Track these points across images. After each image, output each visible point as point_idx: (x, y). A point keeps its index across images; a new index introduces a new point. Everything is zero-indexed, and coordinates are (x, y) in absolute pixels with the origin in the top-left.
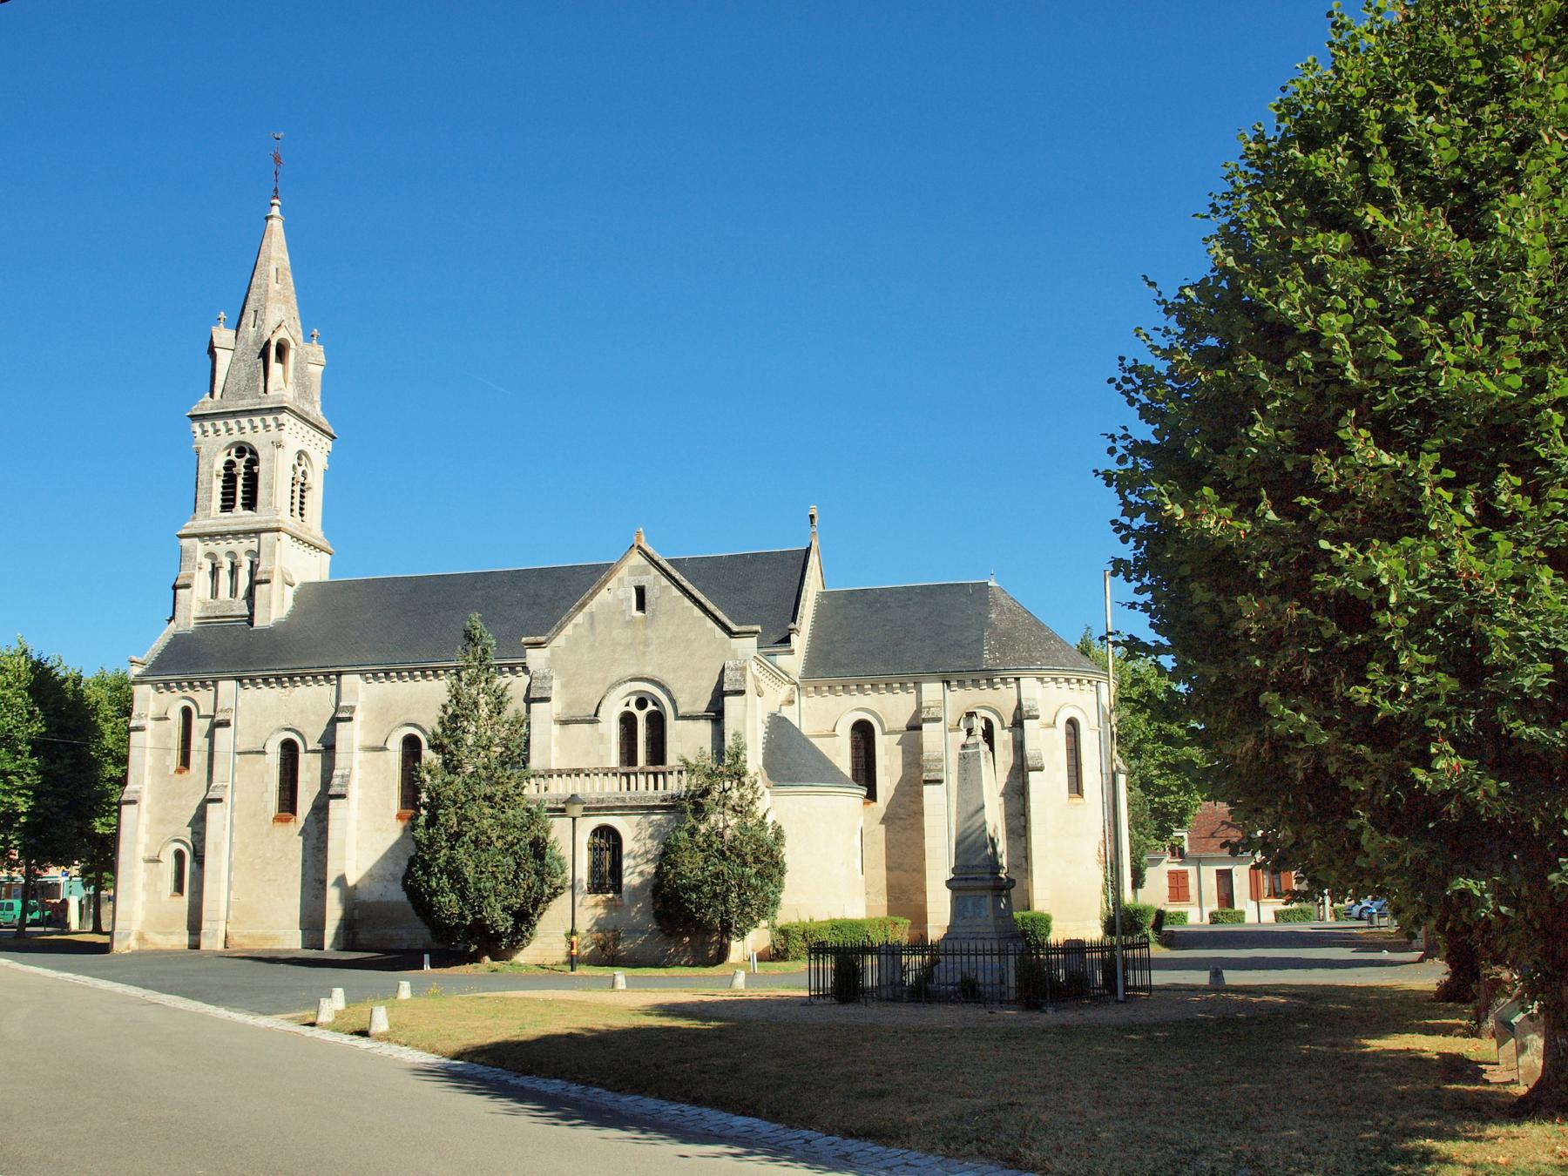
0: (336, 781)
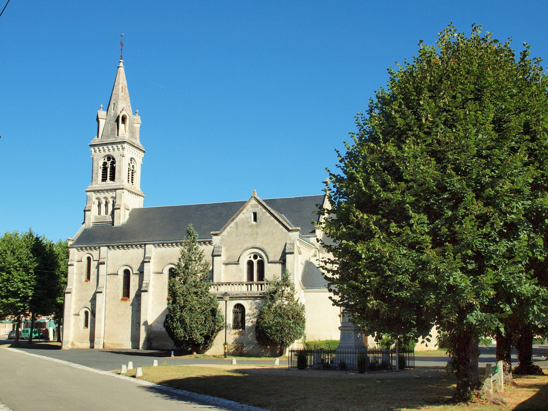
0: (144, 285)
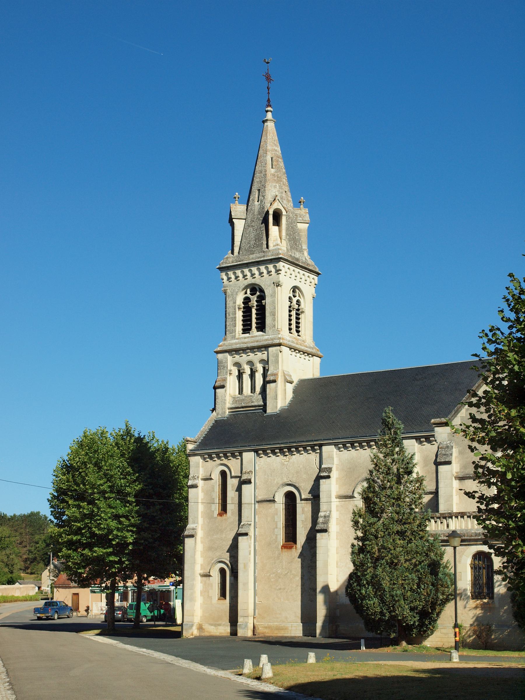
0: (320, 520)
